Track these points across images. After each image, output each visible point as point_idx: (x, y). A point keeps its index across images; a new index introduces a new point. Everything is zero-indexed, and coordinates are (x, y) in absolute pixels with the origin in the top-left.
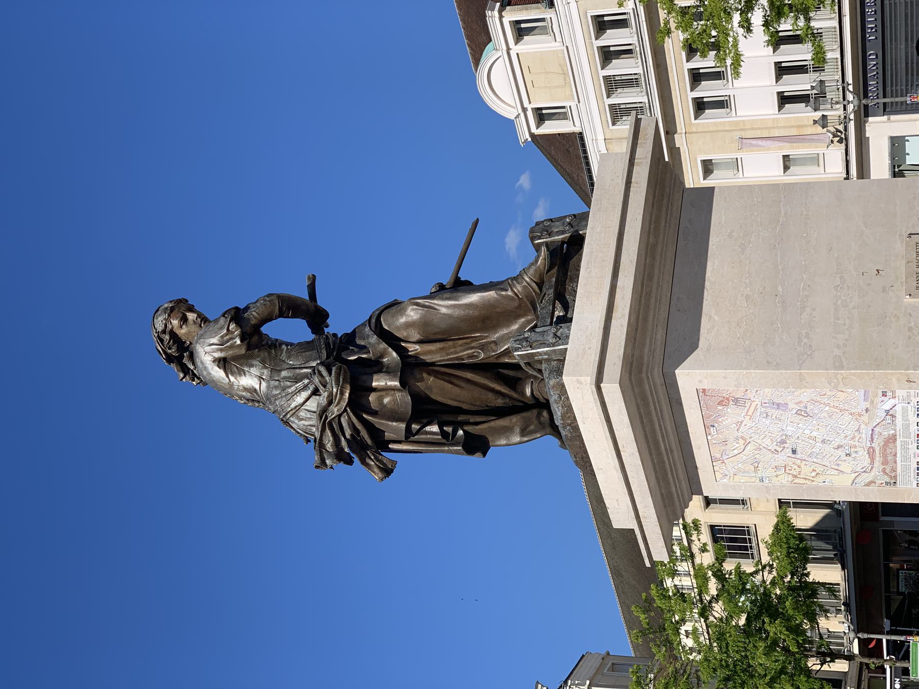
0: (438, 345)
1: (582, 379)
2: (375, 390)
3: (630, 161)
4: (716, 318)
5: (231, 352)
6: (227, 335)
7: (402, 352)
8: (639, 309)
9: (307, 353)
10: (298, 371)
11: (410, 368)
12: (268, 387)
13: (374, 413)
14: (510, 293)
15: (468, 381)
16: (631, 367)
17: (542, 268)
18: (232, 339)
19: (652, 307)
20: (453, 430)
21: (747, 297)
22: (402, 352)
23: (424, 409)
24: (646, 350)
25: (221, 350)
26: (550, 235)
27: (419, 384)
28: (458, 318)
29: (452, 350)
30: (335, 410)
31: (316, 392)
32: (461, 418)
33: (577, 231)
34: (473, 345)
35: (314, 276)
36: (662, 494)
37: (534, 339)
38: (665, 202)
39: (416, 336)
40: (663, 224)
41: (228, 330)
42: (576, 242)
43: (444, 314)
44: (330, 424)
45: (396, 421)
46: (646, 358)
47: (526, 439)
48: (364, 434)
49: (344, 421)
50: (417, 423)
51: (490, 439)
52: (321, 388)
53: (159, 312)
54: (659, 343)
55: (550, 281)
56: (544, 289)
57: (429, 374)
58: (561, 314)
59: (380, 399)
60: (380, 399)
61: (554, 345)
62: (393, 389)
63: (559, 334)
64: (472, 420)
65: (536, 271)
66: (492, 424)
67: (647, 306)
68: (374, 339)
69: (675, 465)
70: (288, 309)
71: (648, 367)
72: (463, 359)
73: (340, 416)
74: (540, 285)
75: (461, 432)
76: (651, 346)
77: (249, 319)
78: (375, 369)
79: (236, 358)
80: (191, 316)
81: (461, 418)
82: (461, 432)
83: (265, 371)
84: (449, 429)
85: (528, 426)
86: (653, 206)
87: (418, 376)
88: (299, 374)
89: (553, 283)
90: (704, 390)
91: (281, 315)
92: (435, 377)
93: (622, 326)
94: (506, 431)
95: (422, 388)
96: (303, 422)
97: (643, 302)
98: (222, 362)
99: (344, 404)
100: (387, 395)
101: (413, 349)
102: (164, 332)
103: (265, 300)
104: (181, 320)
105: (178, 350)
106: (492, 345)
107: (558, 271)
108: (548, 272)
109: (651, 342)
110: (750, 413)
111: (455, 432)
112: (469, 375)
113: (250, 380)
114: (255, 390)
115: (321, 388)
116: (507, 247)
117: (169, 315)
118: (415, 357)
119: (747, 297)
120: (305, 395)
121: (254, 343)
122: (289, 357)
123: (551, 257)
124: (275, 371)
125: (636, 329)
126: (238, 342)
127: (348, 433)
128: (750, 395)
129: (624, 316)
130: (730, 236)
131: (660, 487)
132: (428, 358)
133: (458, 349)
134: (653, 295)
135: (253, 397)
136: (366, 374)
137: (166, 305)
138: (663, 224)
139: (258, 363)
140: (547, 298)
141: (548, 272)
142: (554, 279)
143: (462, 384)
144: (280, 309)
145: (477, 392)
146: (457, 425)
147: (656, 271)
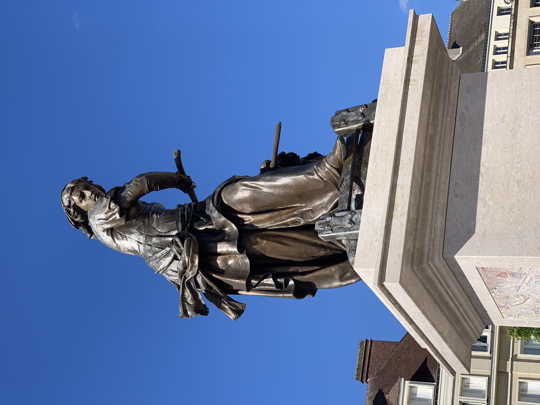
0: (267, 215)
1: (370, 270)
2: (220, 254)
3: (408, 59)
4: (491, 203)
5: (114, 224)
6: (109, 212)
7: (239, 222)
8: (420, 200)
9: (170, 223)
10: (163, 239)
11: (246, 236)
12: (145, 250)
13: (221, 272)
14: (316, 177)
15: (295, 240)
16: (413, 257)
17: (339, 157)
18: (113, 214)
19: (431, 197)
20: (285, 281)
21: (519, 182)
22: (239, 222)
23: (261, 266)
24: (427, 240)
25: (107, 223)
26: (347, 124)
27: (255, 247)
28: (279, 195)
29: (278, 218)
30: (190, 274)
31: (175, 258)
32: (292, 269)
33: (368, 121)
34: (295, 213)
35: (179, 152)
36: (457, 332)
37: (334, 223)
38: (443, 92)
39: (248, 209)
40: (441, 114)
41: (109, 208)
42: (368, 129)
43: (267, 193)
44: (189, 283)
45: (238, 279)
46: (426, 248)
47: (344, 283)
48: (215, 288)
49: (199, 279)
50: (255, 279)
51: (316, 284)
52: (178, 255)
53: (64, 191)
54: (439, 230)
55: (347, 168)
56: (342, 174)
57: (262, 238)
58: (359, 193)
59: (225, 261)
60: (225, 261)
61: (349, 230)
62: (234, 253)
63: (354, 219)
64: (300, 271)
65: (334, 160)
66: (316, 274)
67: (427, 195)
68: (215, 214)
69: (466, 313)
70: (156, 185)
71: (428, 256)
72: (288, 225)
73: (195, 277)
74: (340, 171)
75: (292, 282)
76: (431, 234)
77: (125, 198)
78: (220, 237)
79: (120, 228)
80: (88, 193)
81: (292, 269)
82: (292, 282)
83: (142, 237)
84: (281, 280)
85: (346, 273)
86: (431, 97)
87: (253, 241)
88: (163, 242)
89: (350, 169)
90: (483, 268)
91: (150, 189)
92: (268, 240)
93: (402, 225)
94: (329, 278)
95: (258, 249)
96: (171, 277)
97: (423, 192)
98: (110, 231)
99: (196, 269)
100: (230, 257)
101: (248, 219)
102: (69, 206)
103: (136, 181)
104: (80, 197)
105: (82, 218)
106: (310, 213)
107: (354, 157)
108: (345, 159)
109: (431, 230)
110: (527, 281)
111: (287, 282)
112: (295, 235)
113: (131, 243)
114: (136, 251)
115: (178, 255)
116: (401, 6)
117: (71, 194)
118: (251, 225)
119: (519, 182)
120: (169, 259)
121: (133, 213)
122: (158, 226)
123: (347, 149)
124: (149, 237)
125: (417, 221)
126: (117, 216)
127: (203, 288)
128: (523, 271)
129: (403, 214)
130: (502, 121)
131: (455, 328)
132: (260, 226)
133: (283, 217)
134: (432, 185)
135: (134, 260)
136: (212, 242)
137: (69, 185)
138: (441, 114)
139: (135, 231)
140: (345, 183)
141: (345, 159)
142: (350, 166)
143: (291, 243)
144: (149, 186)
145: (303, 248)
146: (288, 276)
147: (435, 161)
